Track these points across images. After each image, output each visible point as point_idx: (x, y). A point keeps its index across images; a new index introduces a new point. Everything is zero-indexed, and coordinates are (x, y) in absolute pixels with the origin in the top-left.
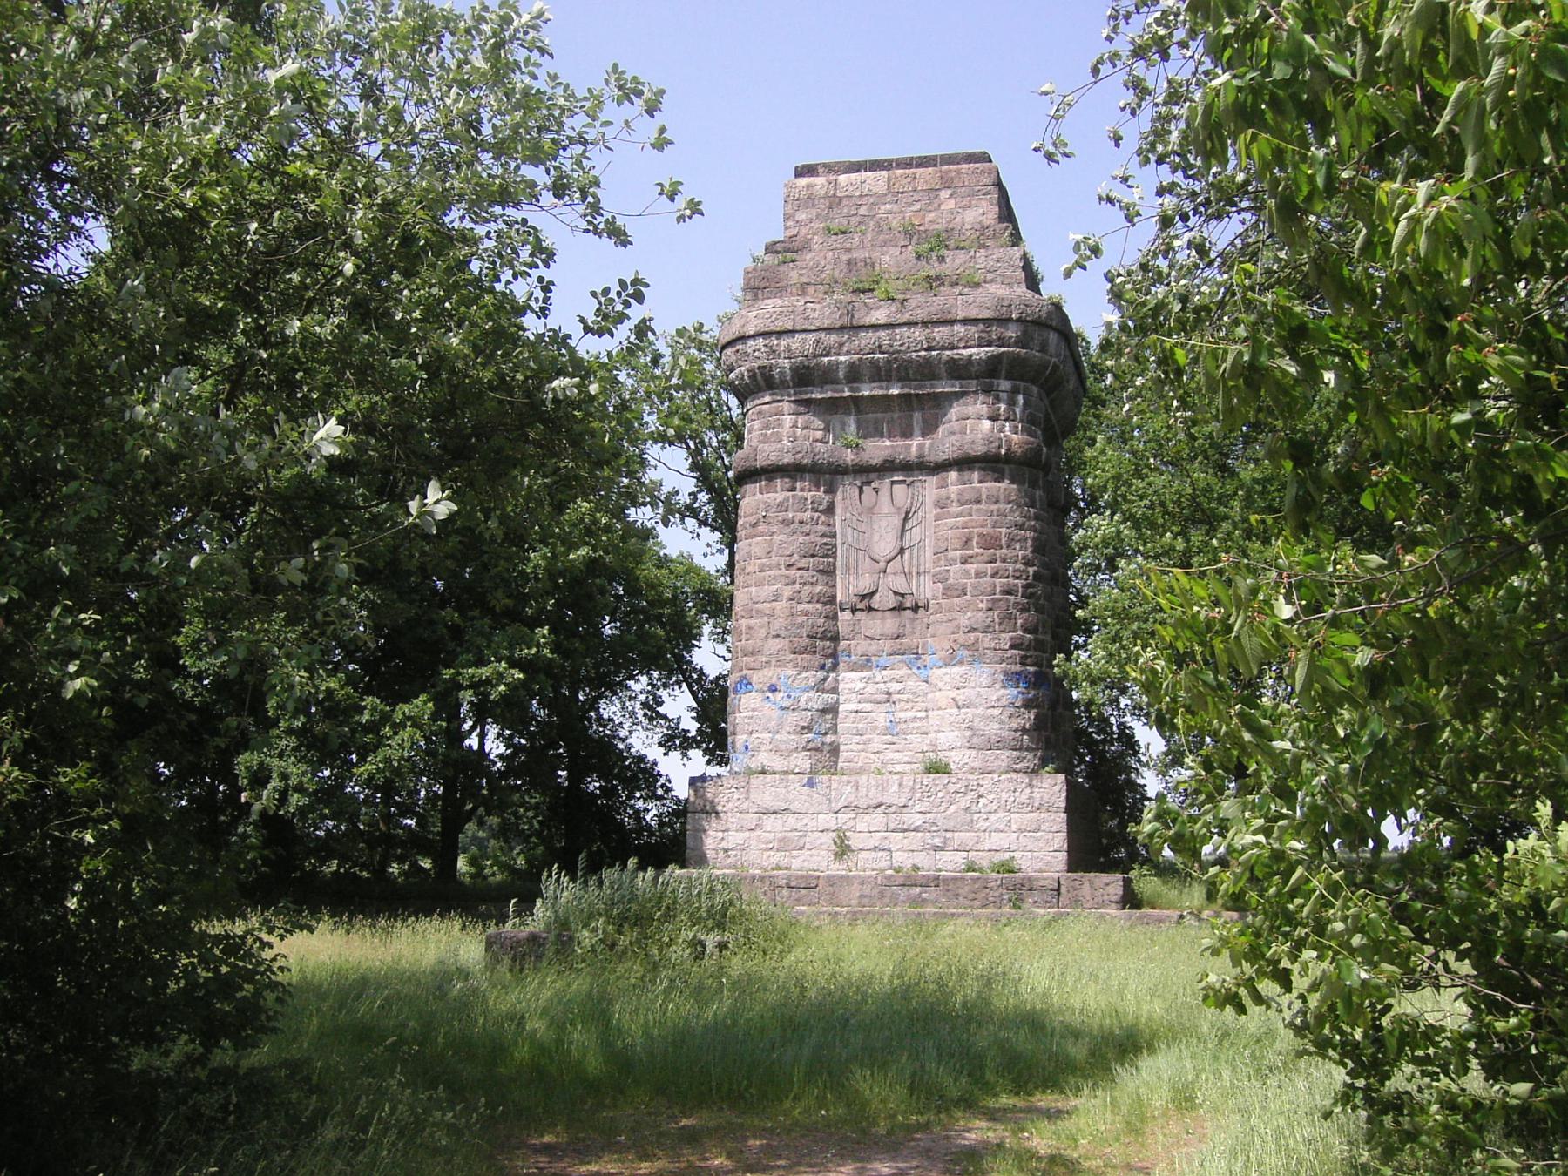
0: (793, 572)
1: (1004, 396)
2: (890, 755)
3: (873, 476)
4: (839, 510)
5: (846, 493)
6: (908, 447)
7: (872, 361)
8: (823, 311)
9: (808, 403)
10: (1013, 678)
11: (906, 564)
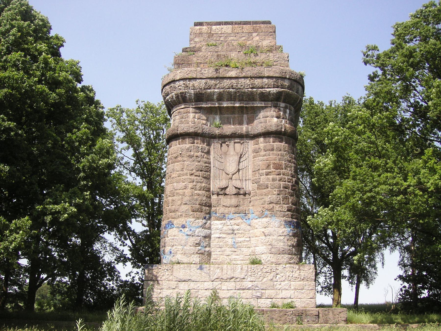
0: (193, 177)
1: (282, 109)
2: (234, 257)
3: (226, 139)
4: (212, 153)
5: (215, 146)
6: (242, 128)
7: (228, 92)
8: (209, 72)
9: (200, 109)
10: (289, 224)
11: (241, 176)
